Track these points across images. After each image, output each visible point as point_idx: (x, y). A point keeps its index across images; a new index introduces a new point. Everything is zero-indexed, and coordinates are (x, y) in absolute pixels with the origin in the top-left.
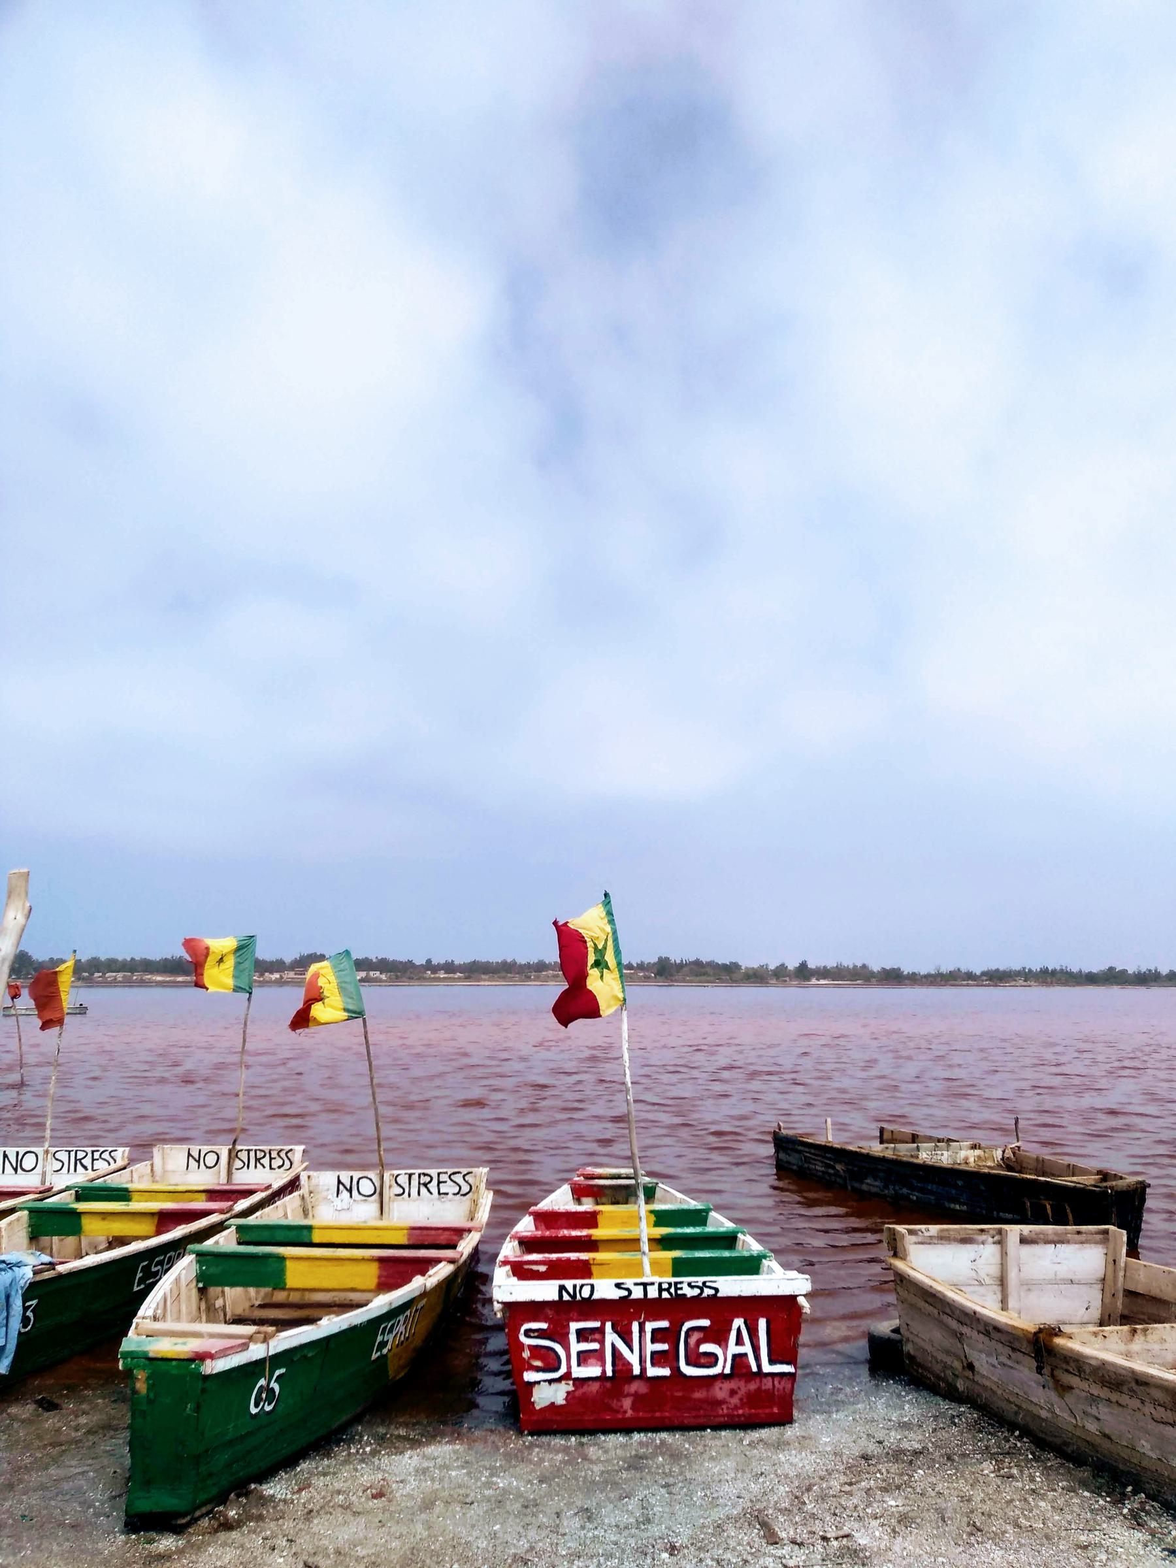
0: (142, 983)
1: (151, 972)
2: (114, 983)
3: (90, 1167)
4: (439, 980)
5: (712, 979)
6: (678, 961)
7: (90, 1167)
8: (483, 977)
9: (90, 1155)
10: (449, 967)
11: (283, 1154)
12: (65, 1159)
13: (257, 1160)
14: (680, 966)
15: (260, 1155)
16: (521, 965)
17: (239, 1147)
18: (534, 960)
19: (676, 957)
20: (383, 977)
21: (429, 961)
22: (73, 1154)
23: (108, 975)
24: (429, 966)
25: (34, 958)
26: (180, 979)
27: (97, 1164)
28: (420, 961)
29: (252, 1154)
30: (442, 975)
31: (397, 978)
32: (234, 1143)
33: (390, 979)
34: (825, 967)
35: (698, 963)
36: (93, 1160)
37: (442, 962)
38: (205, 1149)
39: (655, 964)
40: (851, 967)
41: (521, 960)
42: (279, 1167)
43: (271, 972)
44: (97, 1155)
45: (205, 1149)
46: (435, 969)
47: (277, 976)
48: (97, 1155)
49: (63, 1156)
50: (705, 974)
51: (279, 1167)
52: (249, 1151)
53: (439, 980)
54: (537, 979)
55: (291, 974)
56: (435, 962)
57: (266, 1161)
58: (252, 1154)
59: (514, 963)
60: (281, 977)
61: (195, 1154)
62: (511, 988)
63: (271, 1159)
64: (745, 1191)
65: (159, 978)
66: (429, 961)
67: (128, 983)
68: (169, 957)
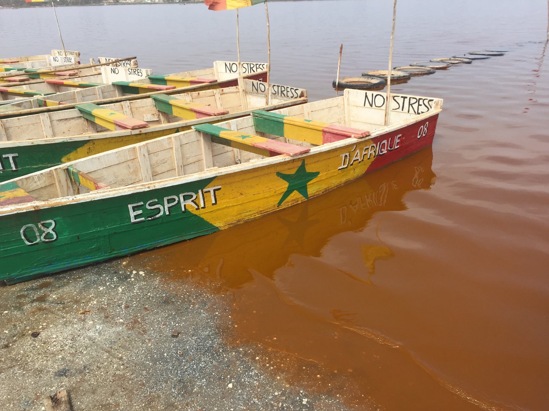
63: (419, 105)
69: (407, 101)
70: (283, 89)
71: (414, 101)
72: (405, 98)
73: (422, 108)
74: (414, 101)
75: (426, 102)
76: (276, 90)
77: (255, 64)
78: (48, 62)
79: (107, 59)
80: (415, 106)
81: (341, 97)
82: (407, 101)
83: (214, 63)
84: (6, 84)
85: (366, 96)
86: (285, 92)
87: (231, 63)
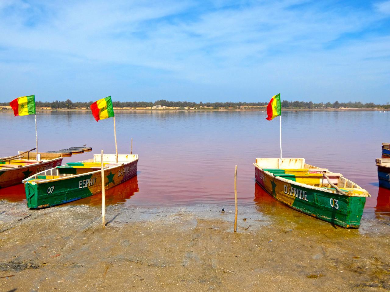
21: (201, 103)
28: (198, 102)
34: (127, 102)
37: (206, 103)
56: (203, 102)
66: (201, 103)
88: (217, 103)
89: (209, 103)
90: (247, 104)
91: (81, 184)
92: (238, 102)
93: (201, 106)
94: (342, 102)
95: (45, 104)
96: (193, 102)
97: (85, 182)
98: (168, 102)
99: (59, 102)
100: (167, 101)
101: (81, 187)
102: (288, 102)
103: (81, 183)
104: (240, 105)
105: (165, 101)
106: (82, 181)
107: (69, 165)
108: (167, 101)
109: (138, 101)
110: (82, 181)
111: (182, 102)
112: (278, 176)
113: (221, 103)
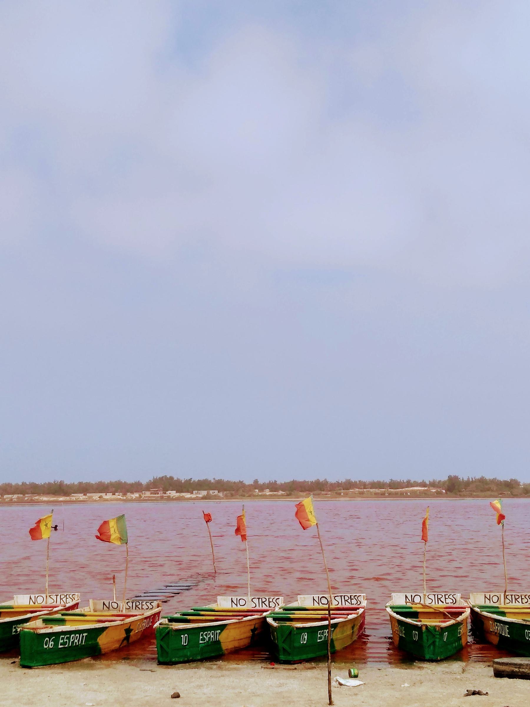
0: (32, 502)
1: (39, 494)
2: (11, 502)
3: (444, 602)
4: (265, 496)
5: (496, 494)
6: (466, 479)
7: (444, 602)
8: (301, 493)
9: (444, 596)
10: (273, 487)
11: (527, 597)
12: (433, 598)
13: (516, 599)
14: (468, 484)
15: (517, 597)
16: (332, 484)
17: (507, 594)
18: (342, 480)
19: (464, 475)
20: (221, 494)
21: (256, 482)
22: (436, 596)
23: (5, 496)
24: (256, 485)
25: (93, 482)
26: (61, 499)
27: (448, 601)
28: (248, 481)
29: (513, 597)
30: (267, 492)
31: (232, 495)
32: (505, 592)
33: (226, 497)
34: (80, 483)
35: (482, 481)
36: (446, 599)
37: (267, 482)
38: (492, 594)
39: (444, 482)
40: (20, 484)
41: (332, 480)
42: (526, 603)
43: (132, 492)
44: (447, 597)
45: (492, 594)
46: (262, 488)
47: (136, 495)
48: (447, 597)
49: (432, 597)
50: (488, 490)
51: (526, 603)
52: (512, 595)
53: (169, 499)
54: (346, 495)
55: (148, 494)
56: (261, 482)
57: (520, 600)
58: (513, 597)
59: (326, 483)
60: (140, 496)
61: (317, 599)
62: (388, 501)
63: (522, 599)
64: (106, 623)
65: (45, 499)
66: (256, 482)
67: (20, 502)
68: (52, 482)
69: (59, 597)
70: (138, 604)
71: (63, 596)
72: (57, 595)
73: (69, 600)
74: (63, 596)
75: (71, 596)
76: (131, 606)
77: (443, 594)
78: (130, 657)
79: (33, 597)
80: (64, 599)
81: (13, 601)
82: (59, 597)
83: (471, 595)
84: (475, 582)
85: (30, 598)
86: (140, 606)
87: (413, 595)
88: (294, 482)
89: (276, 481)
90: (364, 485)
91: (62, 641)
92: (344, 481)
93: (257, 490)
94: (4, 482)
95: (43, 486)
96: (237, 480)
97: (206, 635)
98: (178, 481)
99: (471, 480)
100: (175, 479)
101: (62, 646)
102: (104, 483)
103: (63, 639)
104: (348, 485)
105: (171, 478)
106: (63, 636)
107: (184, 615)
108: (175, 479)
109: (196, 478)
110: (63, 636)
111: (212, 481)
112: (485, 611)
113: (305, 482)
